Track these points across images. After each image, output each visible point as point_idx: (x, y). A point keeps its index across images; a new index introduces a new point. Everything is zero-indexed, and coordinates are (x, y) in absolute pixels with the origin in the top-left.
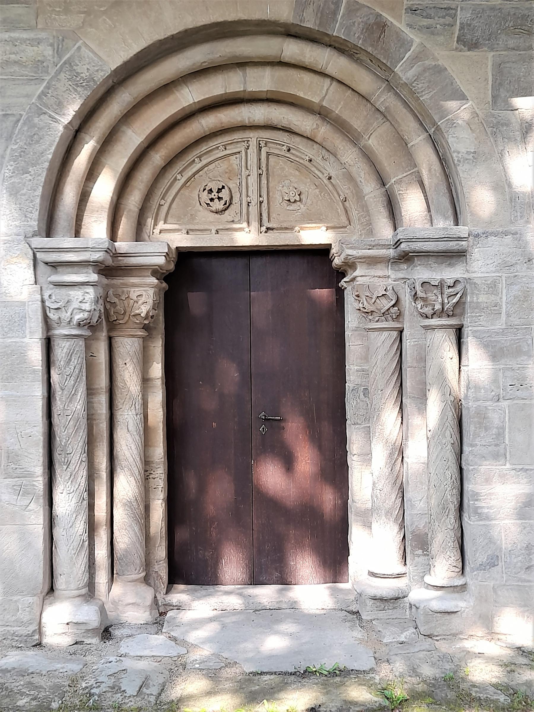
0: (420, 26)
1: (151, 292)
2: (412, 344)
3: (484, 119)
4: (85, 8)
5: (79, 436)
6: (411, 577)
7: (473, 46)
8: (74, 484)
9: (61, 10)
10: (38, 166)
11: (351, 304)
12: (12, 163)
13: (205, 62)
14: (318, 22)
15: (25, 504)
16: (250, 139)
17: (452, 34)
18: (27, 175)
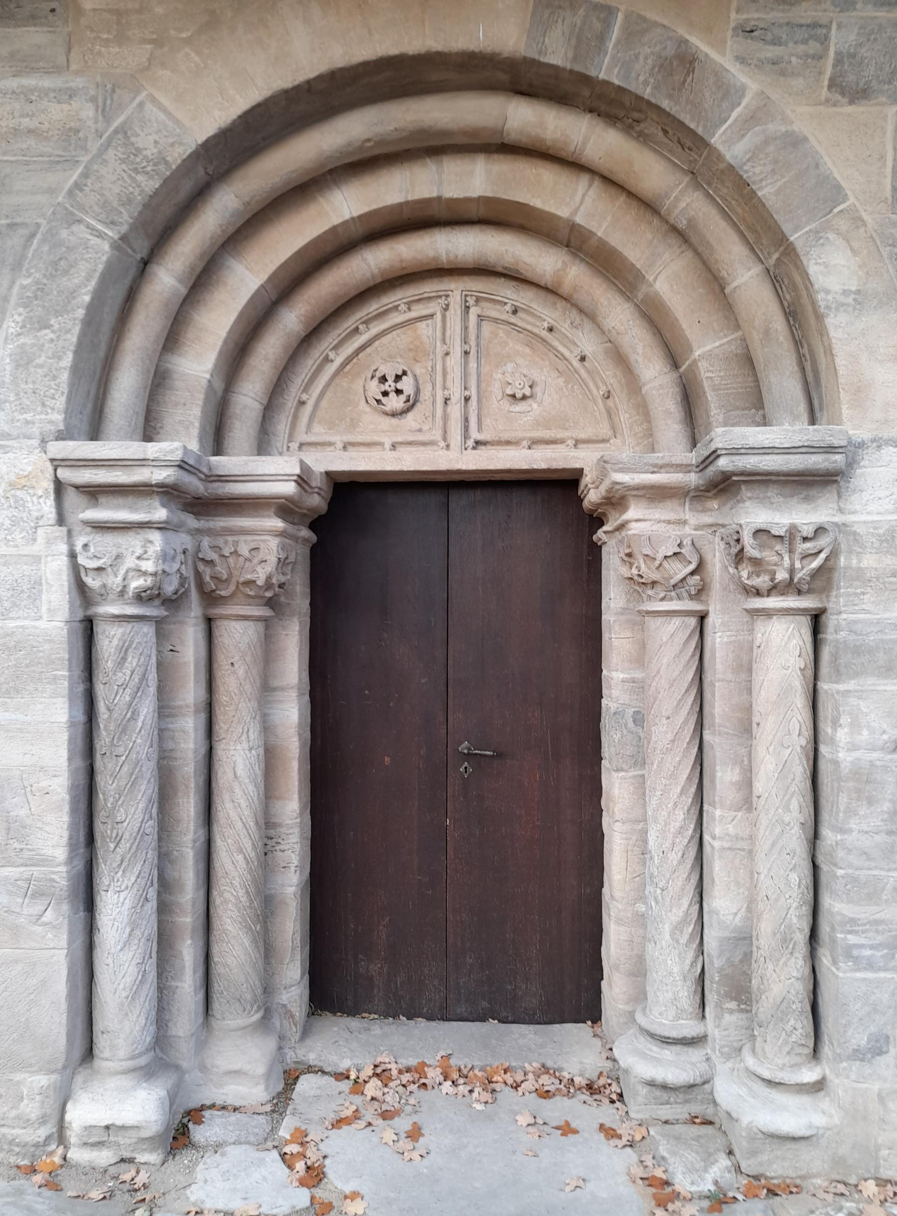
0: (760, 60)
1: (274, 543)
2: (725, 639)
3: (875, 231)
4: (153, 33)
5: (139, 791)
6: (718, 1047)
7: (859, 94)
8: (128, 875)
9: (111, 37)
10: (65, 316)
11: (616, 570)
12: (21, 310)
13: (368, 140)
14: (570, 55)
15: (35, 913)
16: (450, 293)
17: (820, 73)
18: (47, 331)
